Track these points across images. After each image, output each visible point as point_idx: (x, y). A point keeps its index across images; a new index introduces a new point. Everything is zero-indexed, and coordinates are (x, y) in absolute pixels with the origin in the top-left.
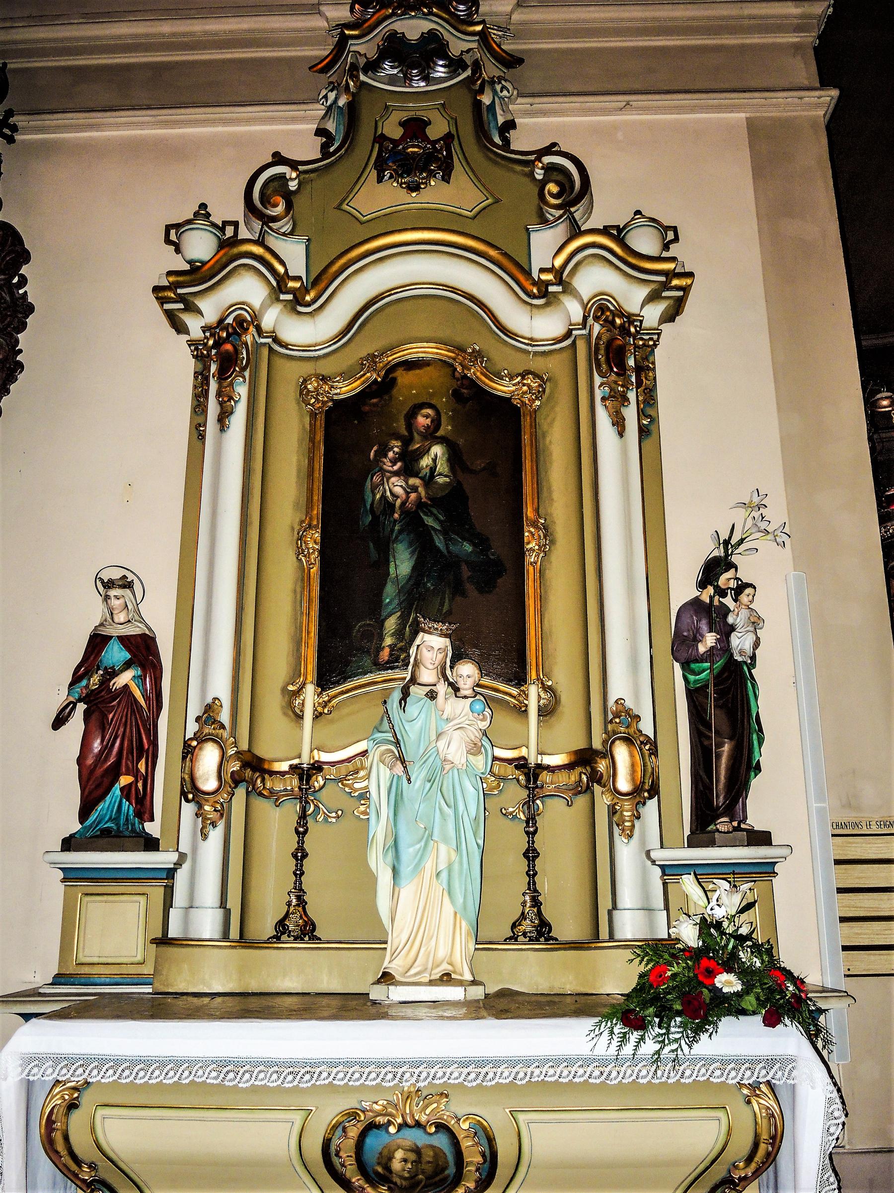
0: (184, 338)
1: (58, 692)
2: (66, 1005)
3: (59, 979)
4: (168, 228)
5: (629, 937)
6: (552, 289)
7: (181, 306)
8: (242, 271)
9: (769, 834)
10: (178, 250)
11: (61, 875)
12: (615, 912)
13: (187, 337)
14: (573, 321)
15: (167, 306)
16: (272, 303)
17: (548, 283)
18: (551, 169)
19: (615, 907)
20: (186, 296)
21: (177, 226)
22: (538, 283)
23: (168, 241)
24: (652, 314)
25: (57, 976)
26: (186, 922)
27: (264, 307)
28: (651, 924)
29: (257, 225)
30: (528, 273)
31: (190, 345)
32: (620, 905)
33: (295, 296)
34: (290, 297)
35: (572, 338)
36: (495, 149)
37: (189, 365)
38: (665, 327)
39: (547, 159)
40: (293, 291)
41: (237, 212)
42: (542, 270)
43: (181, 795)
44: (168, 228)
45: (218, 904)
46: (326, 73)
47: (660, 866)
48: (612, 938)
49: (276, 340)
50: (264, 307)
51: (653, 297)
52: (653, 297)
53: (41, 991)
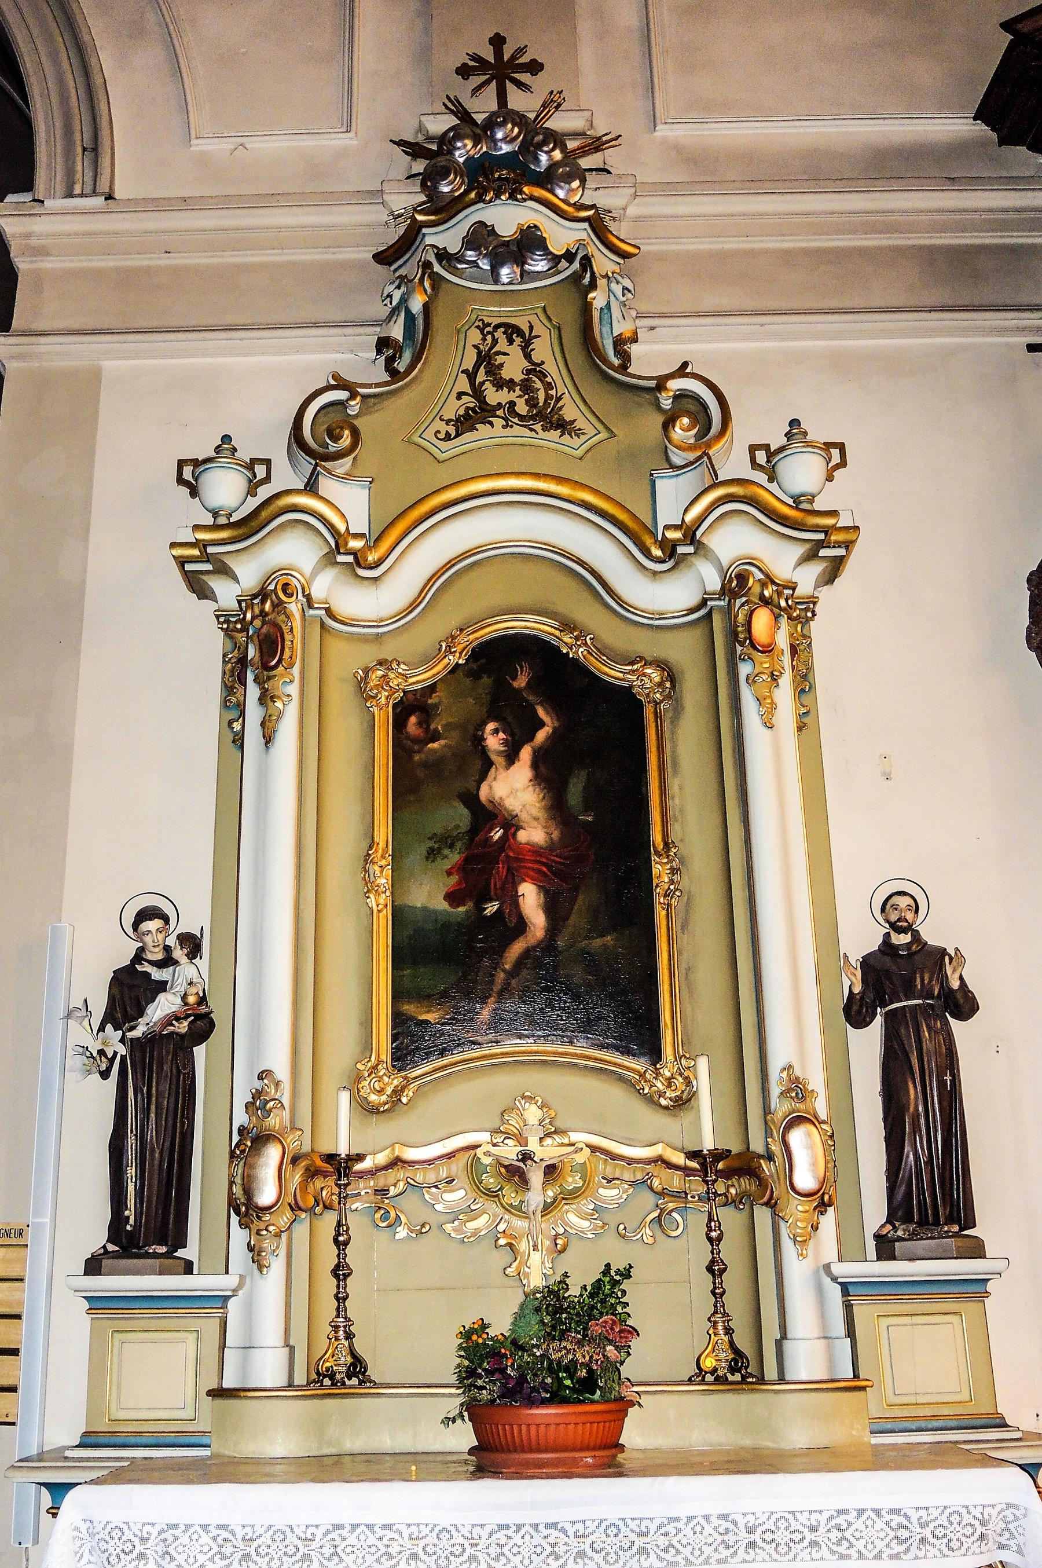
0: (209, 606)
1: (998, 1049)
2: (105, 1472)
3: (89, 1440)
4: (181, 464)
5: (804, 1377)
6: (681, 550)
7: (208, 567)
8: (298, 532)
9: (491, 39)
10: (194, 492)
11: (86, 1305)
12: (785, 1342)
13: (214, 606)
14: (709, 589)
15: (188, 567)
16: (326, 566)
17: (674, 544)
18: (681, 396)
19: (784, 1336)
20: (217, 556)
21: (196, 463)
22: (663, 544)
23: (180, 480)
24: (806, 578)
25: (86, 1434)
26: (244, 1367)
27: (315, 573)
28: (831, 1361)
29: (307, 465)
30: (653, 534)
31: (218, 617)
32: (789, 1336)
33: (356, 558)
34: (350, 559)
35: (708, 608)
36: (604, 367)
37: (215, 642)
38: (825, 594)
39: (675, 385)
40: (354, 553)
41: (278, 452)
42: (667, 527)
43: (230, 1205)
44: (181, 464)
45: (282, 1344)
46: (390, 265)
47: (840, 1284)
48: (782, 1379)
49: (329, 612)
50: (315, 573)
51: (811, 556)
52: (811, 556)
53: (69, 1453)
